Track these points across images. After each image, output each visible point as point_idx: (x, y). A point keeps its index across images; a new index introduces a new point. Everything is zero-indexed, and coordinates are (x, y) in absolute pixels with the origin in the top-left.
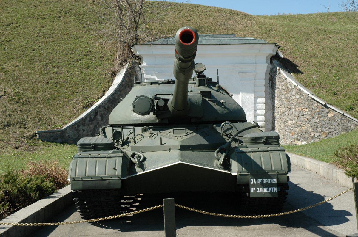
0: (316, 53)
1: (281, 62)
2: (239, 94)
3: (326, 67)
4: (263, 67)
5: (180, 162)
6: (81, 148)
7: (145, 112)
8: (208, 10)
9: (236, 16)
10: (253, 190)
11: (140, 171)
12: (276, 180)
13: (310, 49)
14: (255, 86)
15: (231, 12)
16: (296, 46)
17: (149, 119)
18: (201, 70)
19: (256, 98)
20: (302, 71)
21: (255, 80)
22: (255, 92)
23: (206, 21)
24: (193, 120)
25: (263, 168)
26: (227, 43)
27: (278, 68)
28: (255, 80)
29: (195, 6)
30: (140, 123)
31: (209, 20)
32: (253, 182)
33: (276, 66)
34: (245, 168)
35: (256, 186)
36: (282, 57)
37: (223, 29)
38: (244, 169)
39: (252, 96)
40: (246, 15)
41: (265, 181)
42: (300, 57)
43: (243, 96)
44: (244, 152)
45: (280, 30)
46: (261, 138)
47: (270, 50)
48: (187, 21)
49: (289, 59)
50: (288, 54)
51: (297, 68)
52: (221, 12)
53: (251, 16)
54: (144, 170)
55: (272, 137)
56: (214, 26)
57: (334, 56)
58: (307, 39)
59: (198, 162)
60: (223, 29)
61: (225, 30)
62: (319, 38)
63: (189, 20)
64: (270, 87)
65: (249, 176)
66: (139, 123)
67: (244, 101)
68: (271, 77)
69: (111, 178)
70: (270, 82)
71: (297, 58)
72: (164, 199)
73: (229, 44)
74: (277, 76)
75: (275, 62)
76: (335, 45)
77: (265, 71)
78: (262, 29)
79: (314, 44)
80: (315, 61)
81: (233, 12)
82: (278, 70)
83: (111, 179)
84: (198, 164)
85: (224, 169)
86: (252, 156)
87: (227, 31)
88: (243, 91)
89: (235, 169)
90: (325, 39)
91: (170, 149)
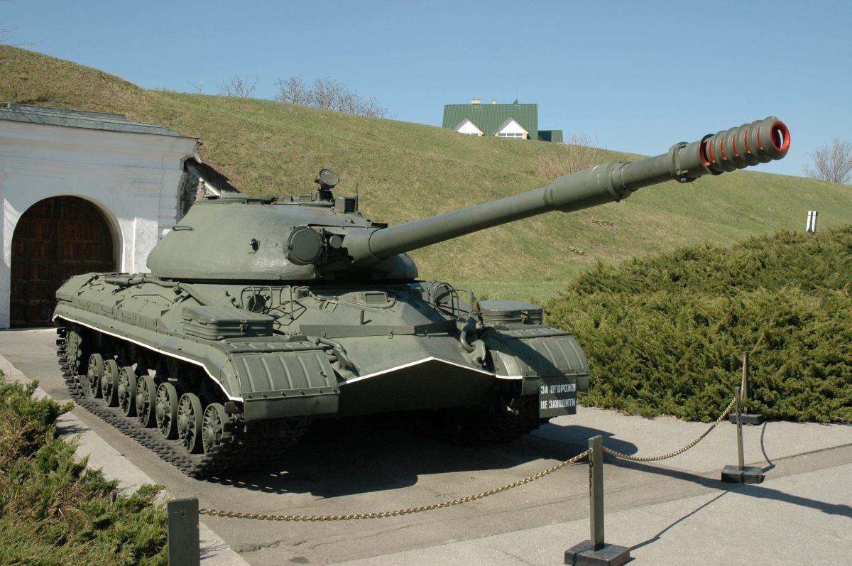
0: (252, 160)
1: (197, 171)
2: (131, 219)
3: (273, 185)
4: (175, 177)
5: (431, 358)
6: (218, 330)
7: (307, 259)
8: (58, 65)
9: (110, 84)
10: (543, 405)
11: (350, 377)
12: (574, 386)
13: (243, 153)
14: (160, 207)
15: (101, 75)
16: (218, 145)
17: (298, 271)
18: (331, 183)
19: (161, 228)
20: (237, 187)
21: (160, 196)
22: (159, 218)
23: (58, 84)
24: (375, 277)
25: (556, 365)
26: (113, 129)
27: (201, 180)
28: (160, 196)
29: (32, 55)
30: (279, 278)
31: (65, 84)
32: (545, 390)
33: (197, 175)
34: (532, 367)
35: (548, 397)
36: (200, 161)
37: (93, 102)
38: (530, 368)
39: (155, 225)
40: (127, 84)
41: (562, 388)
42: (230, 165)
43: (140, 224)
44: (516, 339)
45: (187, 116)
46: (519, 313)
47: (187, 149)
48: (23, 81)
49: (212, 166)
50: (209, 158)
51: (228, 182)
52: (86, 73)
53: (136, 87)
54: (358, 376)
55: (535, 310)
56: (75, 95)
57: (280, 167)
58: (234, 136)
59: (450, 357)
60: (93, 102)
61: (97, 105)
62: (252, 136)
63: (25, 79)
64: (182, 210)
65: (538, 382)
66: (274, 278)
67: (141, 231)
68: (186, 193)
69: (321, 392)
70: (183, 202)
71: (224, 165)
72: (592, 439)
73: (120, 132)
74: (198, 192)
75: (191, 168)
76: (278, 150)
77: (177, 184)
78: (165, 113)
79: (247, 145)
80: (255, 175)
81: (105, 75)
82: (200, 184)
83: (320, 394)
84: (451, 360)
85: (484, 368)
86: (530, 343)
87: (102, 107)
88: (139, 216)
89: (510, 369)
90: (260, 140)
91: (392, 333)
